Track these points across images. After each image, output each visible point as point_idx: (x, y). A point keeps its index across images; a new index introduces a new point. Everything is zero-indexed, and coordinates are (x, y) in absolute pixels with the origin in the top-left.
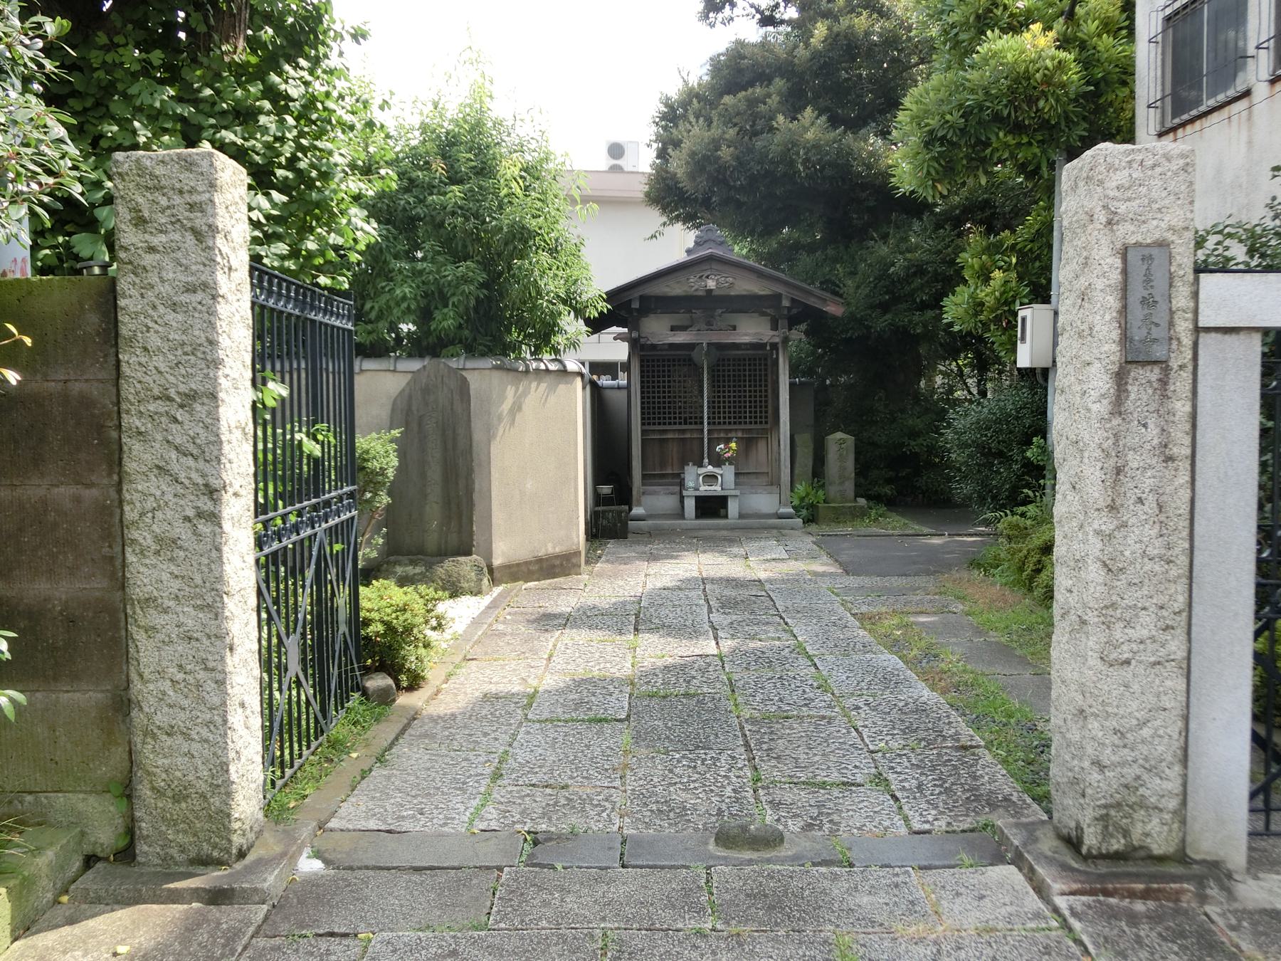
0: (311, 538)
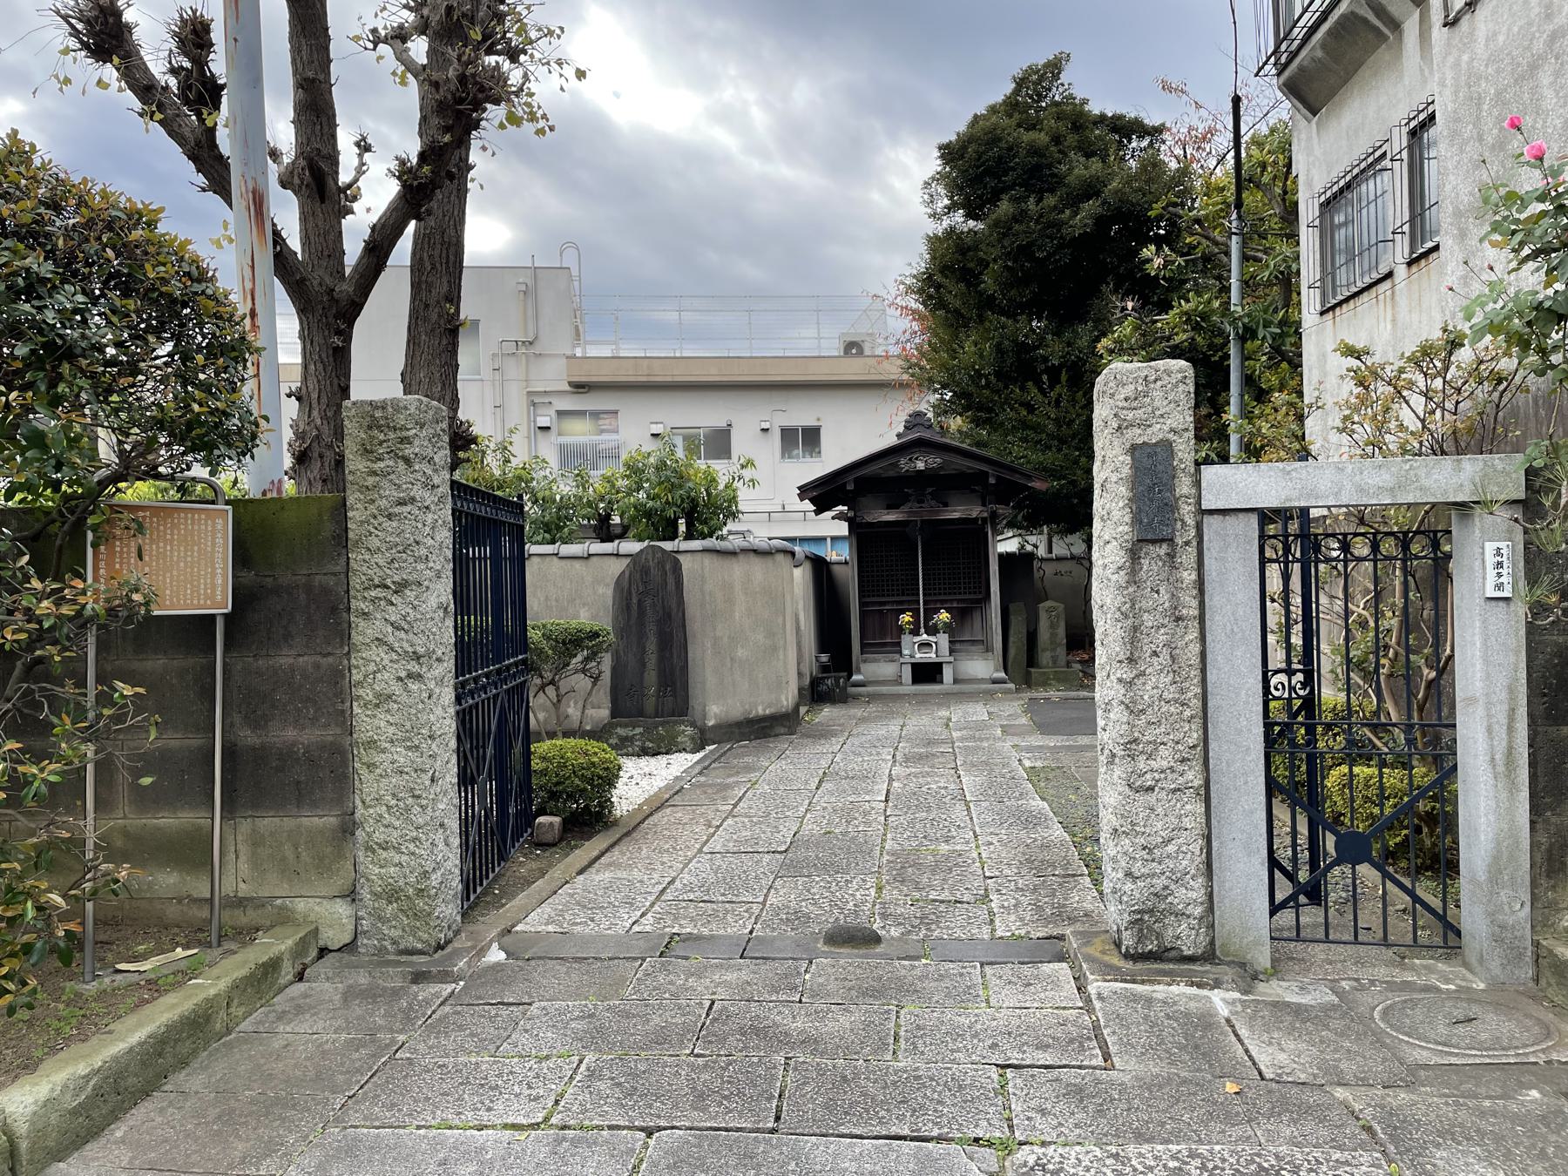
0: (496, 696)
